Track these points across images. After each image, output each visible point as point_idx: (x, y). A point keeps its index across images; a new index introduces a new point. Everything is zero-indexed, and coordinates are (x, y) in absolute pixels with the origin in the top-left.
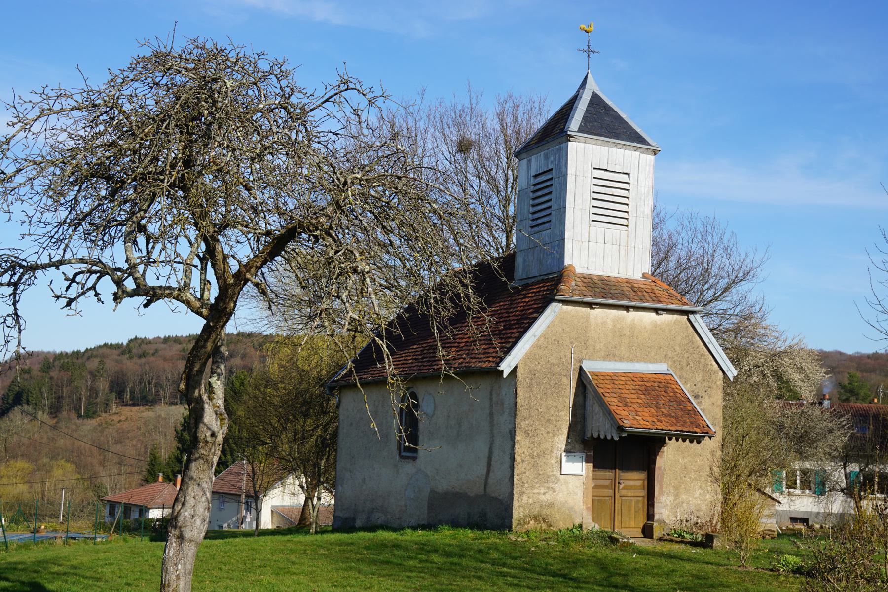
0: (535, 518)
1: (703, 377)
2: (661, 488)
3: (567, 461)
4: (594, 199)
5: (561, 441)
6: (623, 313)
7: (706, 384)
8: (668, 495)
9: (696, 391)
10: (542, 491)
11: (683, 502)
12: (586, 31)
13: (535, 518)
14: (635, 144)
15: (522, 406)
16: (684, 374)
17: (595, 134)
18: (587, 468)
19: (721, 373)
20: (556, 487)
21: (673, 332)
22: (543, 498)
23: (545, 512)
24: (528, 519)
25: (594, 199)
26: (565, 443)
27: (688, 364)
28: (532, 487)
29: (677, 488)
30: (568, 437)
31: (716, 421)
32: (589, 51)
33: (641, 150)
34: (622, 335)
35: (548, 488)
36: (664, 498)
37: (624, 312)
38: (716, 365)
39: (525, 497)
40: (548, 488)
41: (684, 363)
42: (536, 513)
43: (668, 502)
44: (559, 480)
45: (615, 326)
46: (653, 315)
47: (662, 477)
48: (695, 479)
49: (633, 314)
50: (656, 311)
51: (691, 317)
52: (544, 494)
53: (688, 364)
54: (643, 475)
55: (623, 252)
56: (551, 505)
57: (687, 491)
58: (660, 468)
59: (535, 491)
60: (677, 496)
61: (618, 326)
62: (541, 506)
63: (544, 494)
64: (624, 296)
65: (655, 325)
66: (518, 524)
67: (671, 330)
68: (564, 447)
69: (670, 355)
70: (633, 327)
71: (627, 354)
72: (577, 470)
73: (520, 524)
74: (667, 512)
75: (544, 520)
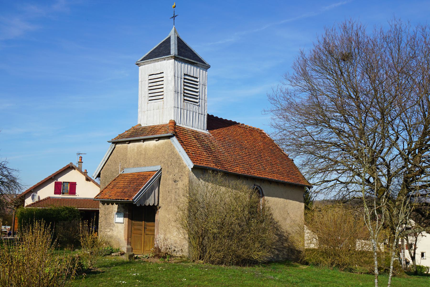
6: (141, 143)
7: (180, 174)
29: (165, 231)
41: (169, 164)
44: (115, 225)
46: (154, 142)
49: (146, 143)
56: (111, 237)
57: (170, 232)
58: (157, 220)
65: (155, 146)
69: (163, 161)
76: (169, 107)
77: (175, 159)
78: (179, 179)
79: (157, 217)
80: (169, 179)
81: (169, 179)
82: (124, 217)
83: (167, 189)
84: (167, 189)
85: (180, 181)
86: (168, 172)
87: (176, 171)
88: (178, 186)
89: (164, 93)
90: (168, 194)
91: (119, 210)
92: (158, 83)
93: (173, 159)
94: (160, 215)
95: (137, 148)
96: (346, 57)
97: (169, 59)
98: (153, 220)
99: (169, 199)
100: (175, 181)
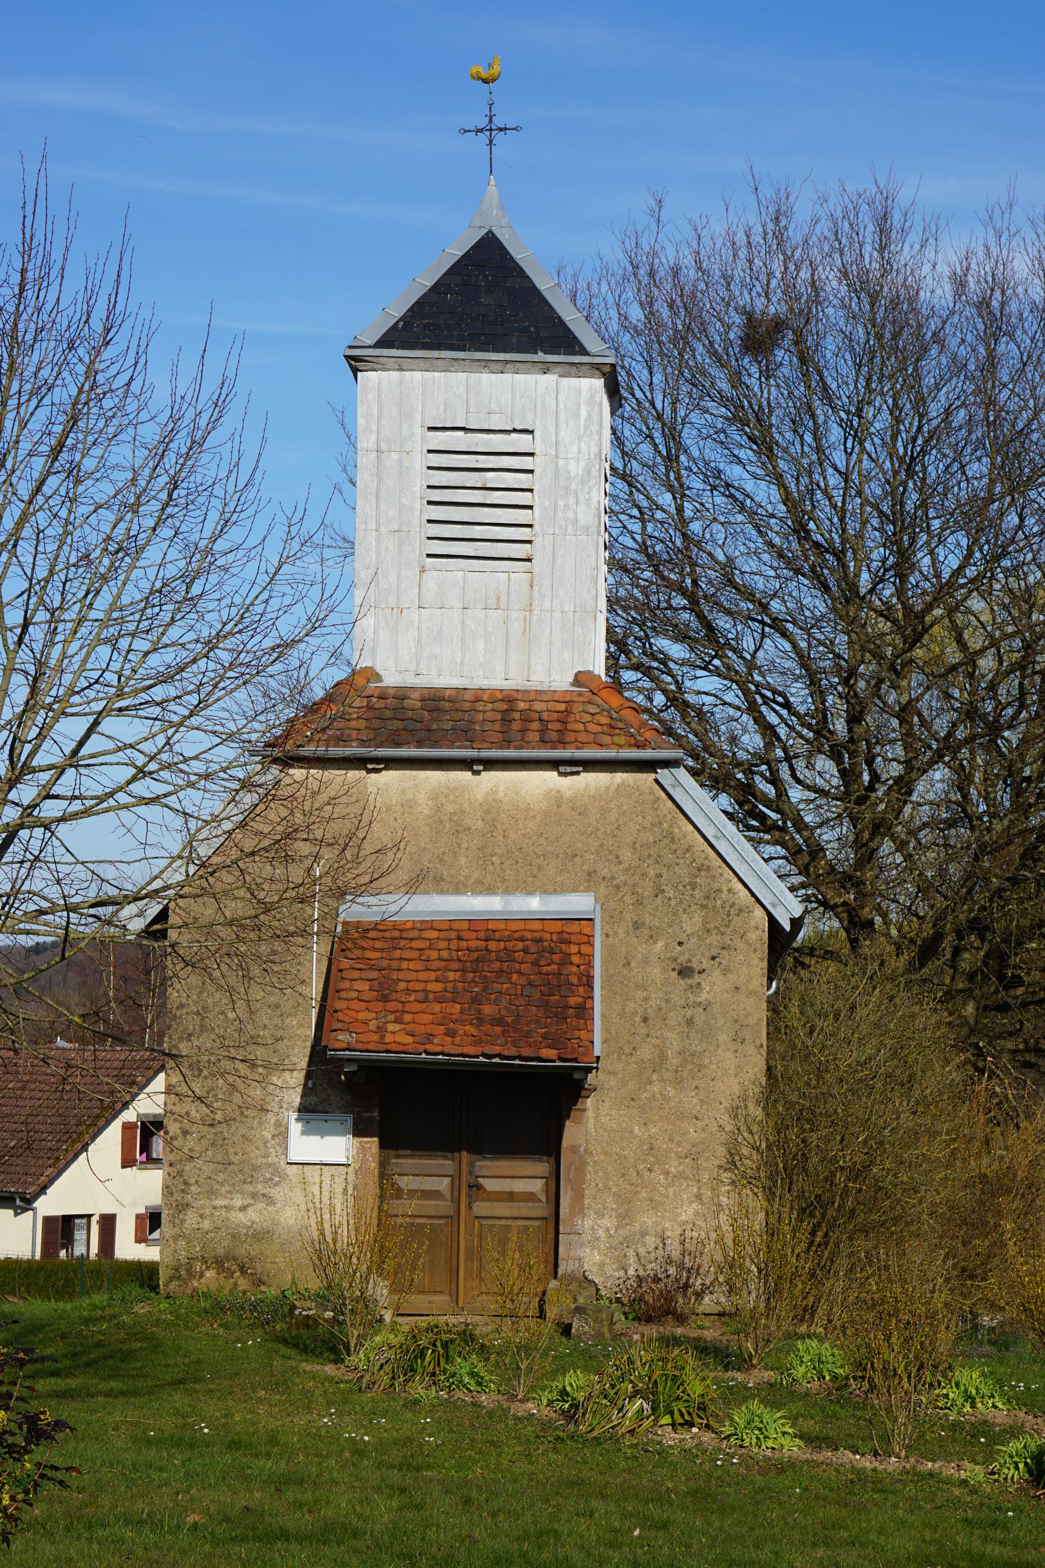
0: (219, 1263)
1: (705, 922)
2: (579, 1196)
3: (304, 1133)
4: (429, 503)
5: (290, 1087)
6: (464, 776)
7: (714, 939)
8: (600, 1215)
9: (682, 959)
10: (238, 1203)
11: (644, 1233)
12: (486, 81)
13: (219, 1263)
14: (540, 356)
15: (181, 1006)
16: (648, 920)
17: (425, 347)
18: (362, 1149)
19: (759, 912)
20: (275, 1192)
21: (612, 817)
22: (240, 1217)
23: (242, 1250)
24: (198, 1266)
25: (429, 503)
26: (299, 1090)
27: (659, 892)
28: (212, 1193)
29: (622, 1199)
30: (308, 1076)
31: (745, 1033)
32: (491, 130)
33: (559, 369)
34: (461, 829)
35: (254, 1195)
36: (588, 1223)
37: (467, 775)
38: (744, 892)
39: (191, 1218)
40: (254, 1195)
41: (647, 889)
42: (220, 1251)
43: (601, 1232)
44: (284, 1177)
45: (438, 808)
46: (550, 777)
47: (581, 1170)
48: (681, 1175)
49: (491, 778)
50: (554, 764)
51: (663, 774)
52: (243, 1208)
53: (659, 892)
54: (542, 1167)
55: (517, 627)
56: (261, 1235)
57: (654, 1205)
58: (575, 1149)
59: (219, 1202)
60: (625, 1217)
61: (449, 808)
62: (234, 1236)
63: (243, 1208)
64: (466, 735)
65: (557, 799)
66: (172, 1278)
67: (604, 812)
68: (297, 1100)
69: (605, 872)
70: (491, 811)
71: (476, 875)
72: (329, 1152)
73: (179, 1278)
74: (601, 1249)
75: (242, 1269)
76: (568, 607)
77: (682, 871)
78: (706, 963)
79: (572, 1134)
80: (646, 961)
81: (646, 961)
82: (359, 1131)
83: (631, 1006)
84: (631, 1006)
85: (716, 973)
86: (637, 925)
87: (692, 923)
88: (703, 997)
89: (539, 535)
90: (645, 1031)
91: (312, 1100)
92: (492, 479)
93: (669, 867)
94: (594, 1126)
95: (434, 797)
96: (759, 337)
97: (576, 370)
98: (546, 1143)
99: (646, 1053)
100: (684, 972)
